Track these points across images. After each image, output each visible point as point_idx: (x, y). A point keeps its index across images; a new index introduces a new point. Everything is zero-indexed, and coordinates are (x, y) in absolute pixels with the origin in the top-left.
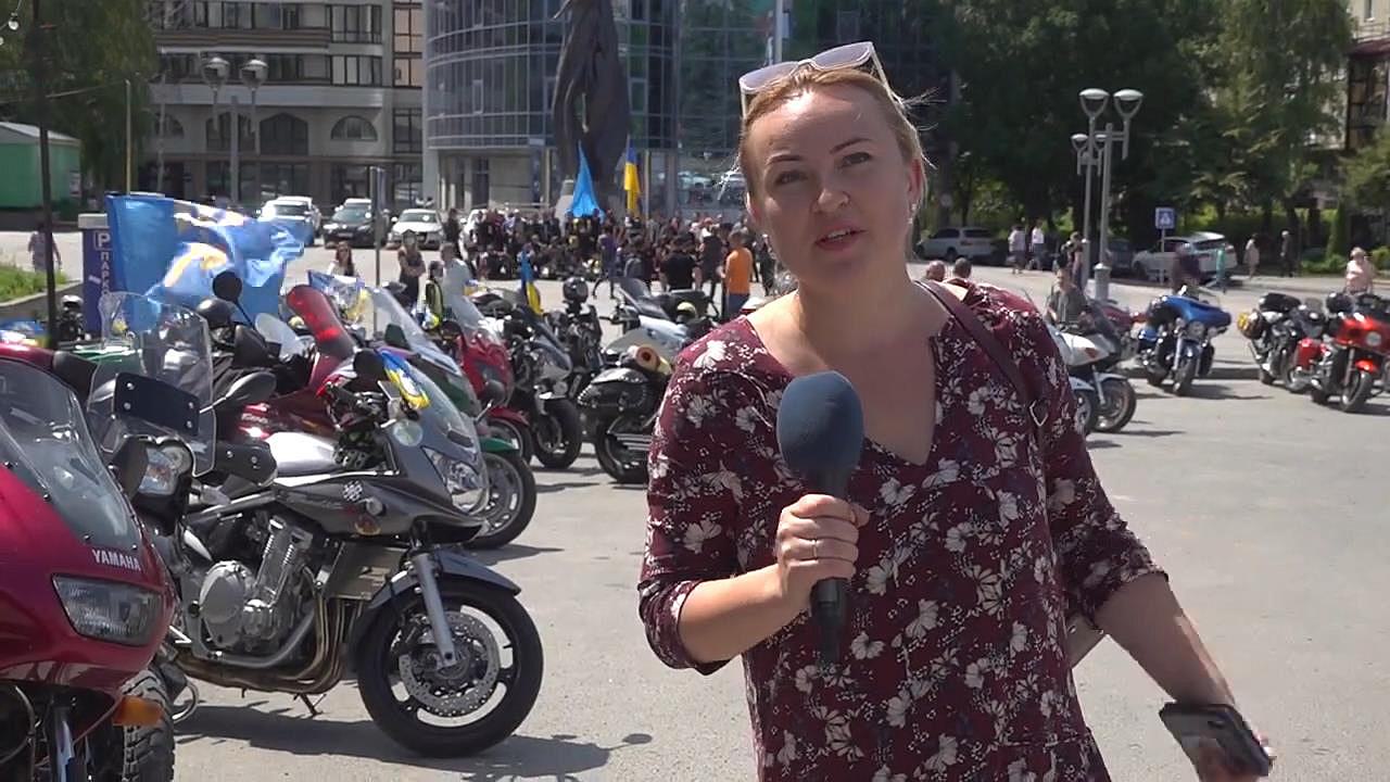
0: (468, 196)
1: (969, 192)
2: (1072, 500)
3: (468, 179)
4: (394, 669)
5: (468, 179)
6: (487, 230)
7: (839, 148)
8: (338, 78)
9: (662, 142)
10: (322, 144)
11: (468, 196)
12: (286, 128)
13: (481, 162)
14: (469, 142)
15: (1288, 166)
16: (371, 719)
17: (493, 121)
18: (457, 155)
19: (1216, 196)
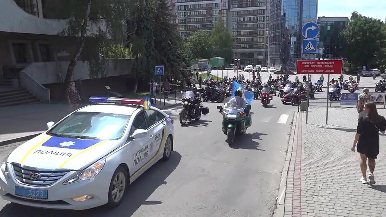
0: (273, 65)
1: (245, 64)
2: (227, 136)
3: (273, 62)
4: (291, 71)
5: (273, 62)
6: (381, 65)
7: (176, 112)
8: (183, 6)
9: (295, 53)
10: (255, 56)
11: (273, 65)
12: (251, 55)
13: (274, 60)
14: (274, 57)
15: (326, 67)
16: (52, 136)
17: (201, 19)
18: (272, 59)
19: (116, 56)
